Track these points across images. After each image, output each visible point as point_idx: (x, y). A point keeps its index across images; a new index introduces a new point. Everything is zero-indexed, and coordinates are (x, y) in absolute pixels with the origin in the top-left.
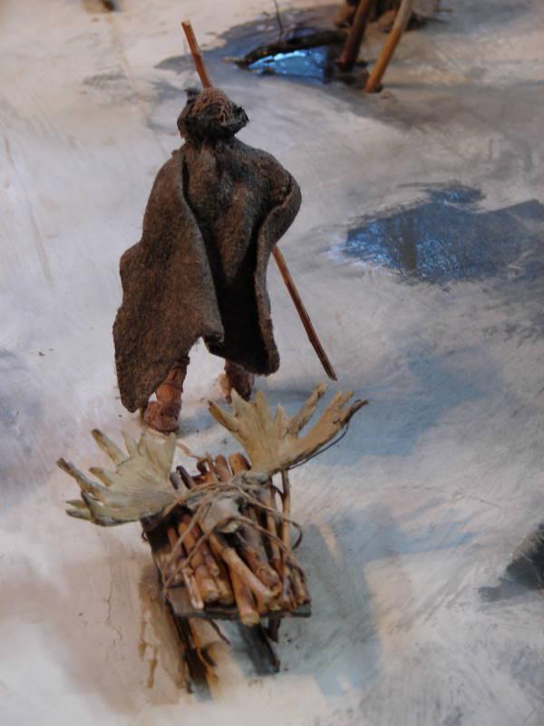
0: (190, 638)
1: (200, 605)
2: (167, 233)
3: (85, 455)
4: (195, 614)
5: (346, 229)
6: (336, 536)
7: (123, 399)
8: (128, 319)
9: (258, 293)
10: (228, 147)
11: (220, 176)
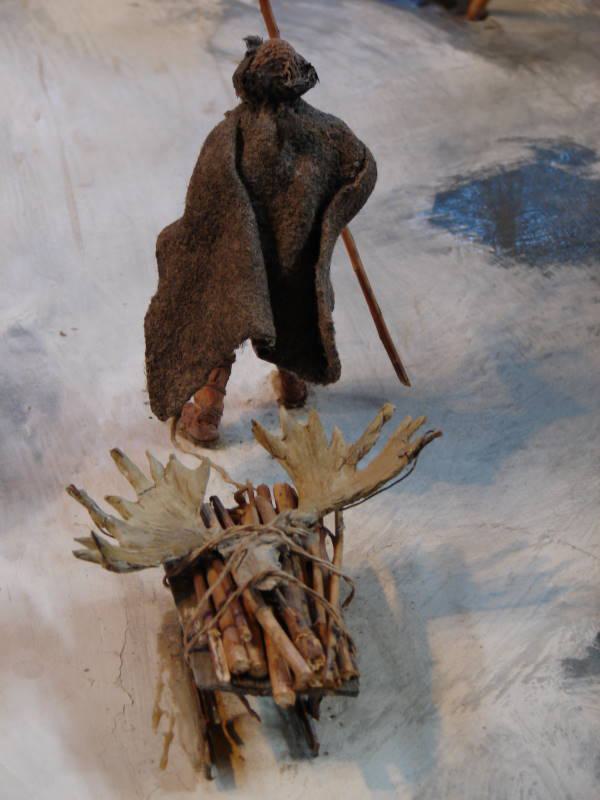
0: (214, 709)
1: (227, 677)
2: (214, 212)
3: (102, 480)
4: (221, 687)
5: (433, 193)
6: (397, 585)
7: (152, 404)
8: (163, 311)
9: (318, 289)
10: (292, 111)
11: (280, 146)
